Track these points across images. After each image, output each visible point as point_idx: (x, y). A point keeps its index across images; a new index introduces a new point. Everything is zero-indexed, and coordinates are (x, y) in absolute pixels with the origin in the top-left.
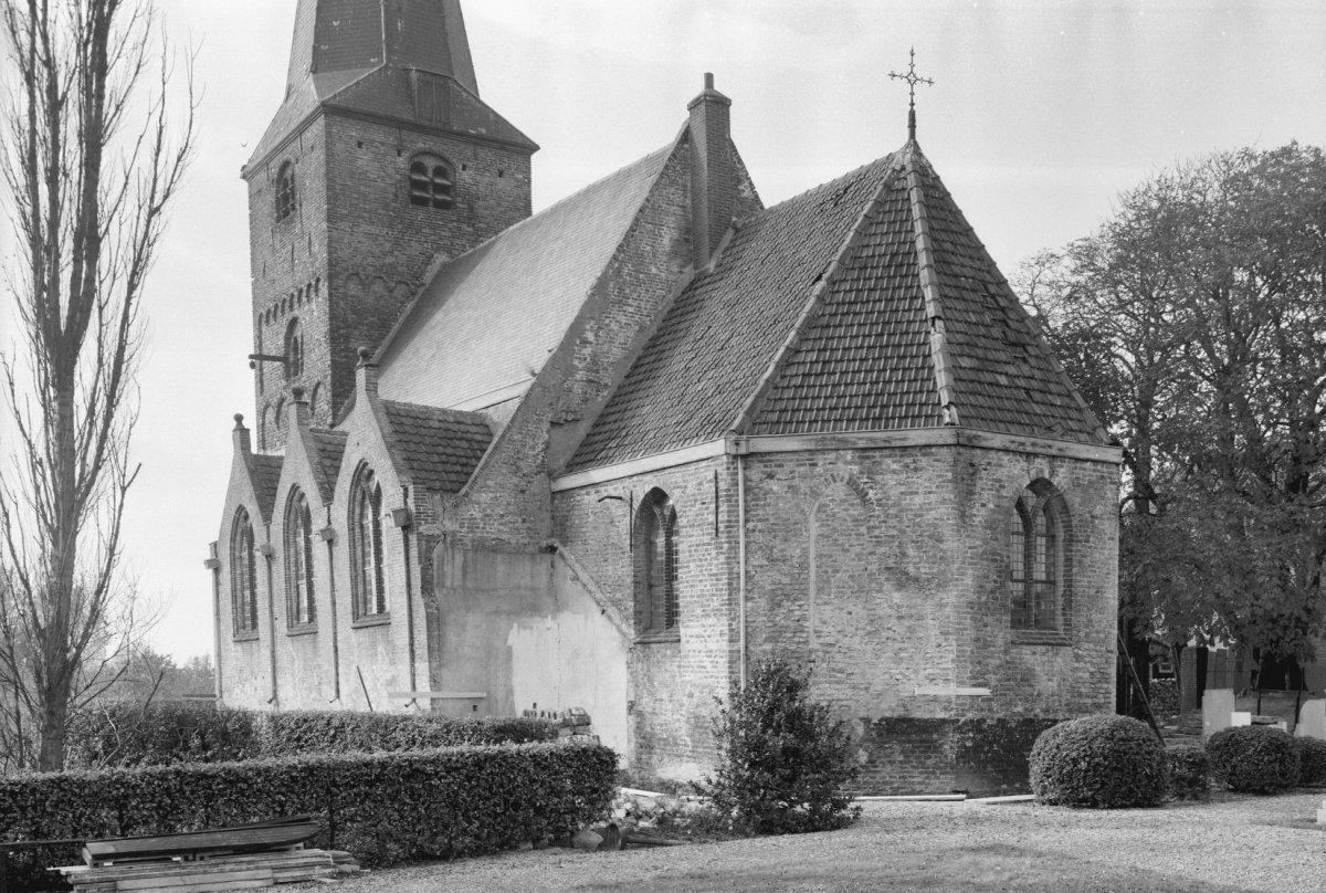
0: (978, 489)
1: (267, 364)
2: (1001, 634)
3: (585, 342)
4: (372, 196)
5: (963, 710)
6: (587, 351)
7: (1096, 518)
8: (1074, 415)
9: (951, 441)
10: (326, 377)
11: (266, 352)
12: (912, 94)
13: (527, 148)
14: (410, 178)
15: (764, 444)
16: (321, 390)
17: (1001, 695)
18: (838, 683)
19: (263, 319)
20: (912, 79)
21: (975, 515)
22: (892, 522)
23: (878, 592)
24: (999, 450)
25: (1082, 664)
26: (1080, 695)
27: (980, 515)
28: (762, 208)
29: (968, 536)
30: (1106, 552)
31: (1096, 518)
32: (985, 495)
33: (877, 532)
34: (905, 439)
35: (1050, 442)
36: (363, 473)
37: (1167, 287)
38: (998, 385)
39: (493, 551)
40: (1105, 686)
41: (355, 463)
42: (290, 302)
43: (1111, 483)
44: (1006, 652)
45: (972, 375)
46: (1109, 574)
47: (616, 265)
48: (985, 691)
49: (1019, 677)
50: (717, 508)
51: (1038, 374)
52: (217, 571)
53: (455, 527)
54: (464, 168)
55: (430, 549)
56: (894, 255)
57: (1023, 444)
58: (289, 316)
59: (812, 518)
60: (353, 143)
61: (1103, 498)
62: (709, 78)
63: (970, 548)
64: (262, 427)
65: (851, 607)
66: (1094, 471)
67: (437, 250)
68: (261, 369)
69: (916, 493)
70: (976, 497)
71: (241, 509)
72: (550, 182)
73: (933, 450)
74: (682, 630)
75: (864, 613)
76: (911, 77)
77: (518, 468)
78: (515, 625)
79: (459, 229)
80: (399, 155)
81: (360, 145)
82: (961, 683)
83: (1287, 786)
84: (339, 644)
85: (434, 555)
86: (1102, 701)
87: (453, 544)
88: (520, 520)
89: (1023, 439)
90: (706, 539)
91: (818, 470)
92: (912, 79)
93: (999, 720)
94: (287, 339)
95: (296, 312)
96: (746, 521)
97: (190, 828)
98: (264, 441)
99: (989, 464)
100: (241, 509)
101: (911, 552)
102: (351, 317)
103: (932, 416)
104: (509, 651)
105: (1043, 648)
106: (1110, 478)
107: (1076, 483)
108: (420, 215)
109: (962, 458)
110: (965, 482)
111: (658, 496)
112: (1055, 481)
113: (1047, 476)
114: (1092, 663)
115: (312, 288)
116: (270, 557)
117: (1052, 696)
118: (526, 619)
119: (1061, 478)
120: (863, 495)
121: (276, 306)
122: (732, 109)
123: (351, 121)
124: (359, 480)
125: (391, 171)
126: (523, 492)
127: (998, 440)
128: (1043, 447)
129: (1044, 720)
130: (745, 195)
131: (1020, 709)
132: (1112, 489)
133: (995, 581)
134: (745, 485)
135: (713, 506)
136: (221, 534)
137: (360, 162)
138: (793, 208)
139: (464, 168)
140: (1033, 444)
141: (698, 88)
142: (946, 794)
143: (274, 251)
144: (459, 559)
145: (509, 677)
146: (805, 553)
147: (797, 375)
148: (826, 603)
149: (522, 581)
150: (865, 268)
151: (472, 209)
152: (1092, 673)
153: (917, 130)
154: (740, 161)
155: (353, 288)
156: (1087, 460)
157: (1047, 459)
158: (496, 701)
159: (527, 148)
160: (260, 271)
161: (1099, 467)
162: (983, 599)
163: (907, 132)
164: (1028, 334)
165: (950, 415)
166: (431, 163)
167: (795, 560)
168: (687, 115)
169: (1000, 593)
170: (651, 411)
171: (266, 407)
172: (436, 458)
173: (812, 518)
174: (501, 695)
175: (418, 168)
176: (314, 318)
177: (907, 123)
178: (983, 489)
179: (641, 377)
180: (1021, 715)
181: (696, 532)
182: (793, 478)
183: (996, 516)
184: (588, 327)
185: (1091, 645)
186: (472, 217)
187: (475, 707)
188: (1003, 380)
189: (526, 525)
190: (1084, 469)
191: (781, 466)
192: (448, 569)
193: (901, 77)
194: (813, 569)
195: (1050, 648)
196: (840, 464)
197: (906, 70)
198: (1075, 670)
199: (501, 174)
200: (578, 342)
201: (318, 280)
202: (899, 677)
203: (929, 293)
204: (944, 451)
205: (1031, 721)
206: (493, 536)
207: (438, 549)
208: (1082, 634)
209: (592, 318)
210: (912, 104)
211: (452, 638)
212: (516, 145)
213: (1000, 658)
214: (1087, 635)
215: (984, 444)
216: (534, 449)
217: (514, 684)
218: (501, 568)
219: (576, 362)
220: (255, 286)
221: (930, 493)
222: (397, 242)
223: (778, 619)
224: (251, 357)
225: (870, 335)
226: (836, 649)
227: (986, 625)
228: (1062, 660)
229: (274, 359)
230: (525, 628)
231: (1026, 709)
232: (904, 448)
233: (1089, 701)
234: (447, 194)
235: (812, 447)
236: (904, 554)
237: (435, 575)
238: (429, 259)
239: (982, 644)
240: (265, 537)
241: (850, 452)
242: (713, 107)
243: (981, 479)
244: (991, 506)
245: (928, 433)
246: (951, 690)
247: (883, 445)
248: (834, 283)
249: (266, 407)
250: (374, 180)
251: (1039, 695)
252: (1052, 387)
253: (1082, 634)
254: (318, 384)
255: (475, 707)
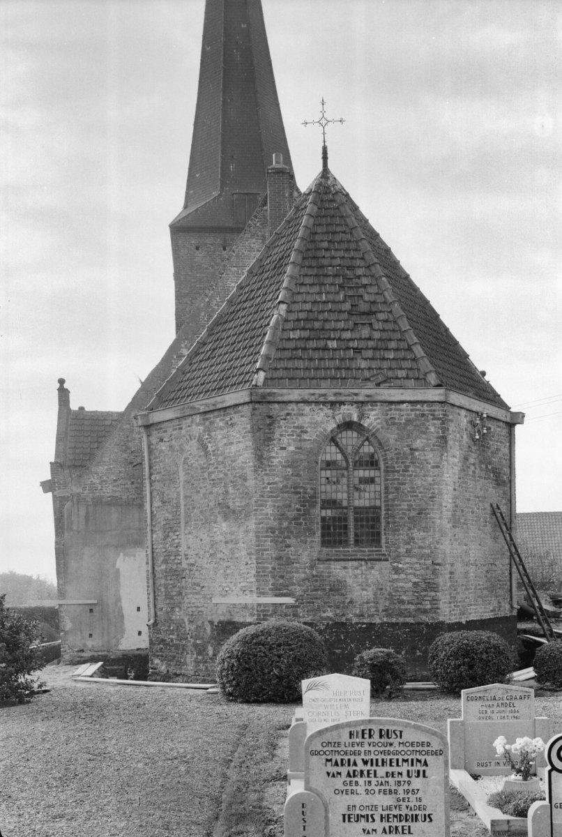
0: (277, 435)
2: (307, 551)
4: (205, 279)
5: (264, 615)
7: (416, 450)
9: (247, 399)
12: (324, 134)
15: (157, 417)
17: (309, 602)
21: (274, 457)
22: (221, 467)
23: (215, 523)
24: (297, 402)
25: (403, 576)
26: (402, 602)
27: (278, 457)
29: (266, 474)
30: (430, 479)
31: (416, 450)
32: (285, 440)
33: (213, 477)
34: (222, 402)
35: (356, 391)
39: (109, 505)
40: (433, 594)
43: (433, 419)
44: (312, 568)
45: (301, 344)
46: (433, 497)
47: (207, 300)
48: (289, 600)
49: (328, 587)
53: (80, 490)
55: (62, 506)
57: (325, 395)
60: (193, 248)
61: (425, 433)
63: (269, 484)
65: (202, 536)
66: (412, 410)
69: (232, 443)
70: (275, 442)
73: (240, 408)
75: (208, 539)
76: (324, 122)
77: (128, 448)
78: (121, 554)
80: (224, 249)
81: (197, 248)
82: (261, 593)
85: (65, 510)
86: (429, 607)
87: (78, 502)
88: (129, 482)
89: (323, 391)
96: (151, 475)
99: (288, 414)
101: (231, 490)
104: (118, 571)
105: (356, 563)
106: (432, 415)
107: (391, 422)
109: (257, 412)
110: (264, 433)
112: (366, 423)
113: (355, 419)
114: (414, 575)
117: (367, 603)
118: (131, 550)
119: (373, 419)
120: (205, 447)
127: (295, 394)
128: (349, 395)
129: (357, 624)
131: (330, 614)
132: (434, 424)
133: (299, 510)
137: (197, 259)
140: (335, 394)
142: (158, 681)
144: (83, 512)
145: (117, 590)
146: (178, 494)
149: (132, 524)
152: (415, 583)
153: (329, 161)
156: (403, 402)
157: (355, 405)
158: (108, 605)
161: (419, 406)
162: (285, 524)
163: (321, 162)
169: (304, 519)
173: (181, 468)
174: (111, 601)
177: (321, 156)
178: (281, 435)
180: (331, 619)
183: (297, 457)
184: (183, 345)
185: (414, 560)
187: (91, 610)
189: (134, 486)
190: (400, 410)
191: (165, 431)
192: (74, 518)
194: (182, 507)
195: (363, 563)
196: (194, 427)
197: (317, 117)
198: (393, 581)
200: (175, 357)
202: (227, 589)
204: (246, 407)
205: (343, 624)
206: (108, 495)
207: (68, 505)
208: (402, 550)
209: (186, 339)
211: (73, 564)
213: (305, 573)
214: (408, 551)
215: (280, 399)
217: (121, 595)
218: (115, 517)
221: (239, 442)
226: (195, 568)
227: (288, 546)
228: (378, 573)
230: (129, 556)
232: (225, 408)
233: (413, 607)
235: (178, 415)
236: (227, 492)
237: (66, 523)
239: (284, 562)
241: (198, 416)
243: (279, 427)
244: (292, 448)
245: (235, 396)
246: (252, 599)
247: (212, 408)
250: (207, 269)
251: (351, 602)
253: (402, 550)
255: (91, 610)
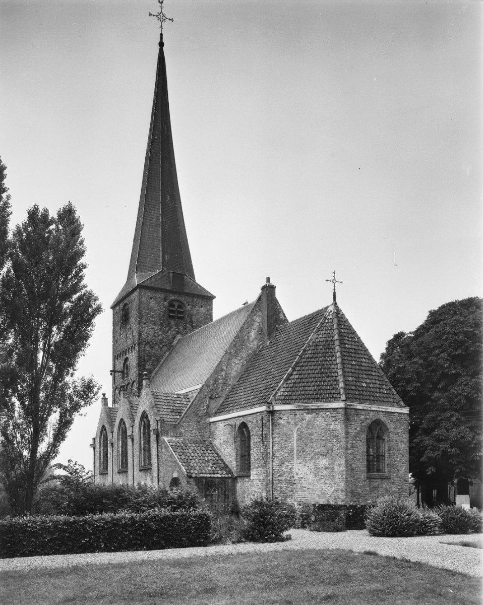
1: (117, 374)
3: (222, 370)
6: (223, 373)
8: (392, 396)
10: (136, 379)
11: (116, 369)
13: (210, 298)
14: (169, 309)
16: (135, 384)
18: (304, 491)
19: (116, 357)
20: (334, 281)
28: (288, 322)
34: (322, 406)
36: (144, 416)
37: (200, 461)
38: (362, 386)
41: (141, 412)
42: (125, 352)
50: (263, 429)
51: (378, 382)
52: (94, 448)
54: (188, 305)
56: (327, 341)
58: (125, 357)
59: (295, 433)
60: (149, 298)
62: (268, 280)
64: (114, 396)
67: (178, 334)
68: (115, 375)
71: (103, 426)
72: (219, 310)
74: (251, 472)
77: (198, 414)
79: (186, 326)
83: (336, 560)
84: (135, 476)
90: (259, 440)
91: (297, 416)
92: (334, 281)
93: (362, 506)
94: (124, 365)
95: (127, 356)
97: (467, 372)
98: (115, 400)
100: (103, 426)
102: (146, 358)
103: (337, 398)
108: (172, 322)
111: (244, 425)
115: (133, 348)
116: (112, 444)
121: (121, 353)
122: (277, 290)
123: (148, 290)
124: (143, 418)
125: (162, 307)
126: (199, 422)
130: (281, 317)
134: (272, 421)
135: (261, 429)
136: (96, 435)
138: (297, 322)
139: (188, 305)
141: (264, 283)
143: (120, 334)
147: (291, 383)
148: (300, 463)
150: (317, 346)
151: (191, 319)
154: (280, 306)
155: (147, 348)
159: (210, 298)
160: (115, 341)
164: (375, 368)
165: (343, 397)
166: (176, 304)
167: (289, 448)
168: (261, 291)
170: (242, 395)
171: (116, 389)
172: (169, 411)
173: (295, 433)
175: (171, 305)
176: (133, 357)
179: (242, 382)
181: (255, 437)
182: (289, 419)
186: (191, 322)
188: (364, 385)
193: (330, 281)
194: (295, 451)
199: (202, 307)
201: (135, 345)
203: (338, 354)
210: (334, 290)
212: (208, 297)
216: (203, 407)
219: (219, 377)
220: (114, 345)
222: (163, 332)
223: (283, 468)
224: (111, 371)
225: (317, 369)
226: (303, 479)
229: (119, 372)
231: (373, 502)
234: (182, 314)
238: (175, 337)
240: (111, 437)
242: (269, 290)
248: (305, 351)
249: (116, 388)
252: (384, 387)
254: (134, 381)
